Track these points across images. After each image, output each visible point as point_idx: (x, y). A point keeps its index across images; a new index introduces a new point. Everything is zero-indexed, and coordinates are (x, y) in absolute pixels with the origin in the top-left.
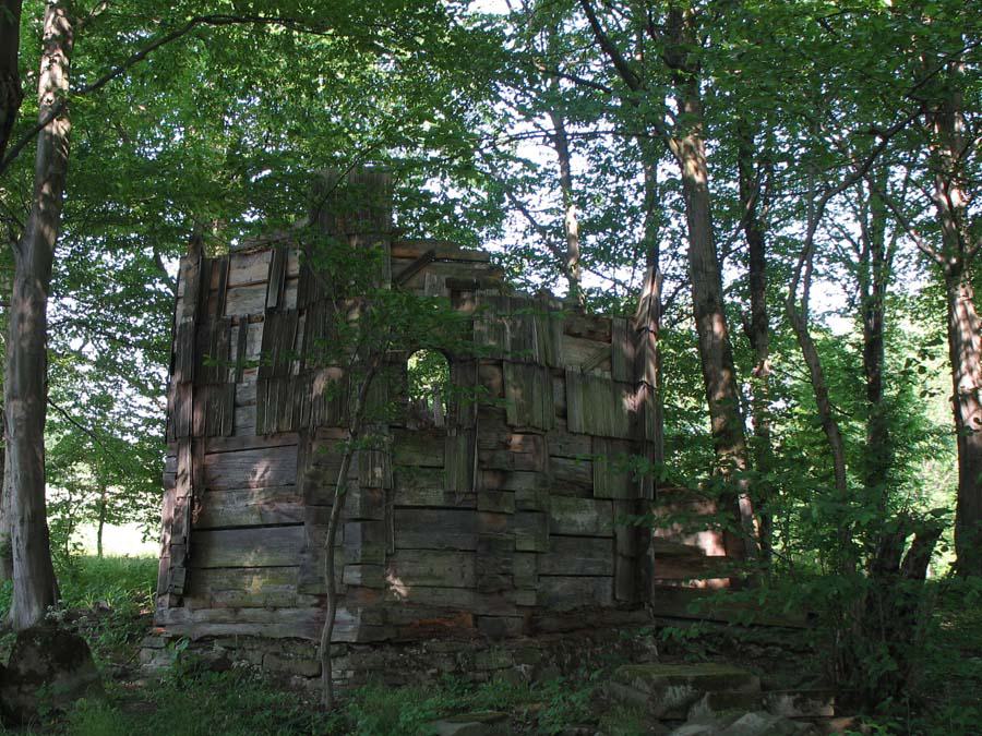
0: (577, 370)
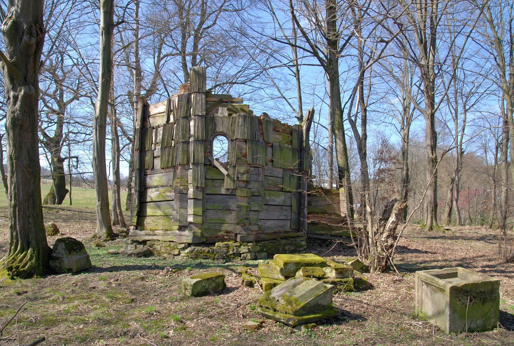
0: (277, 144)
